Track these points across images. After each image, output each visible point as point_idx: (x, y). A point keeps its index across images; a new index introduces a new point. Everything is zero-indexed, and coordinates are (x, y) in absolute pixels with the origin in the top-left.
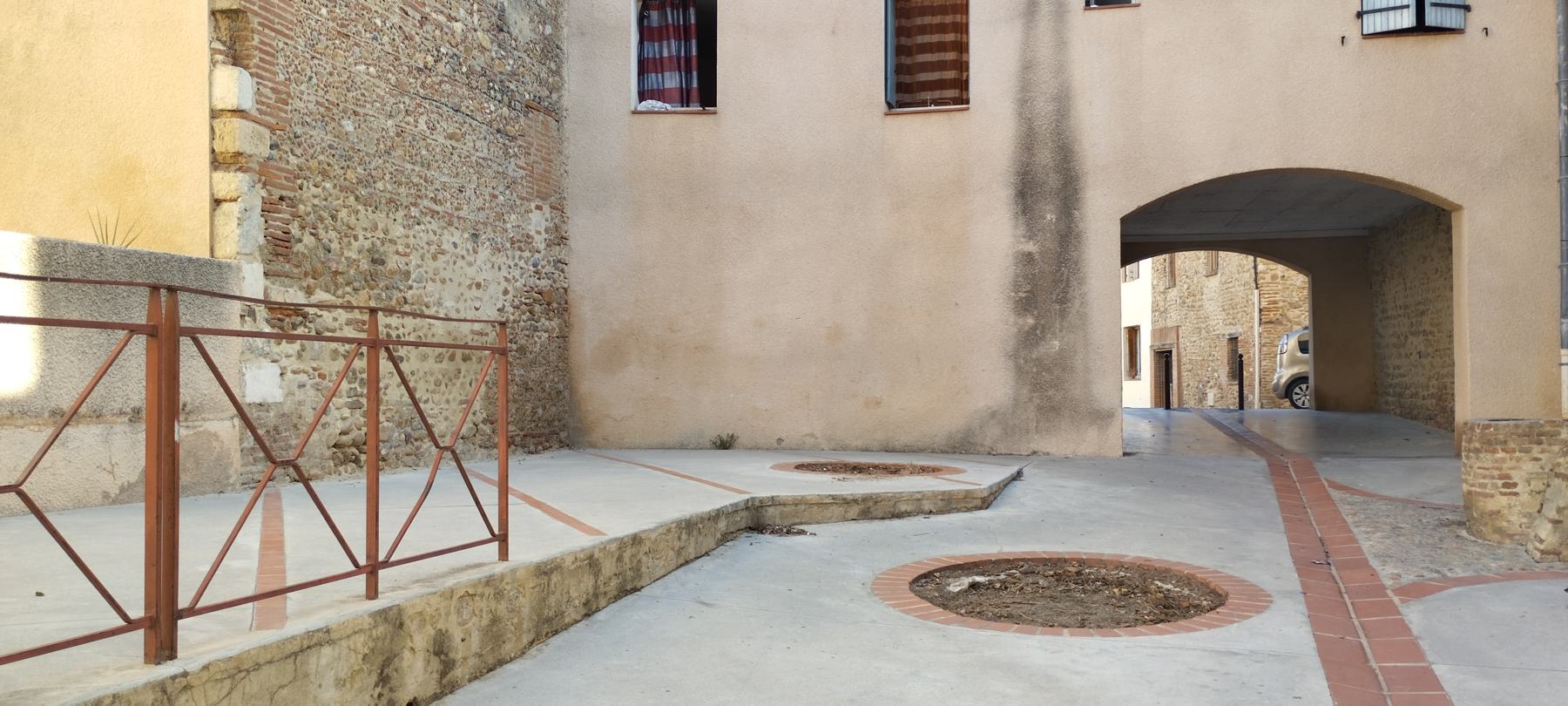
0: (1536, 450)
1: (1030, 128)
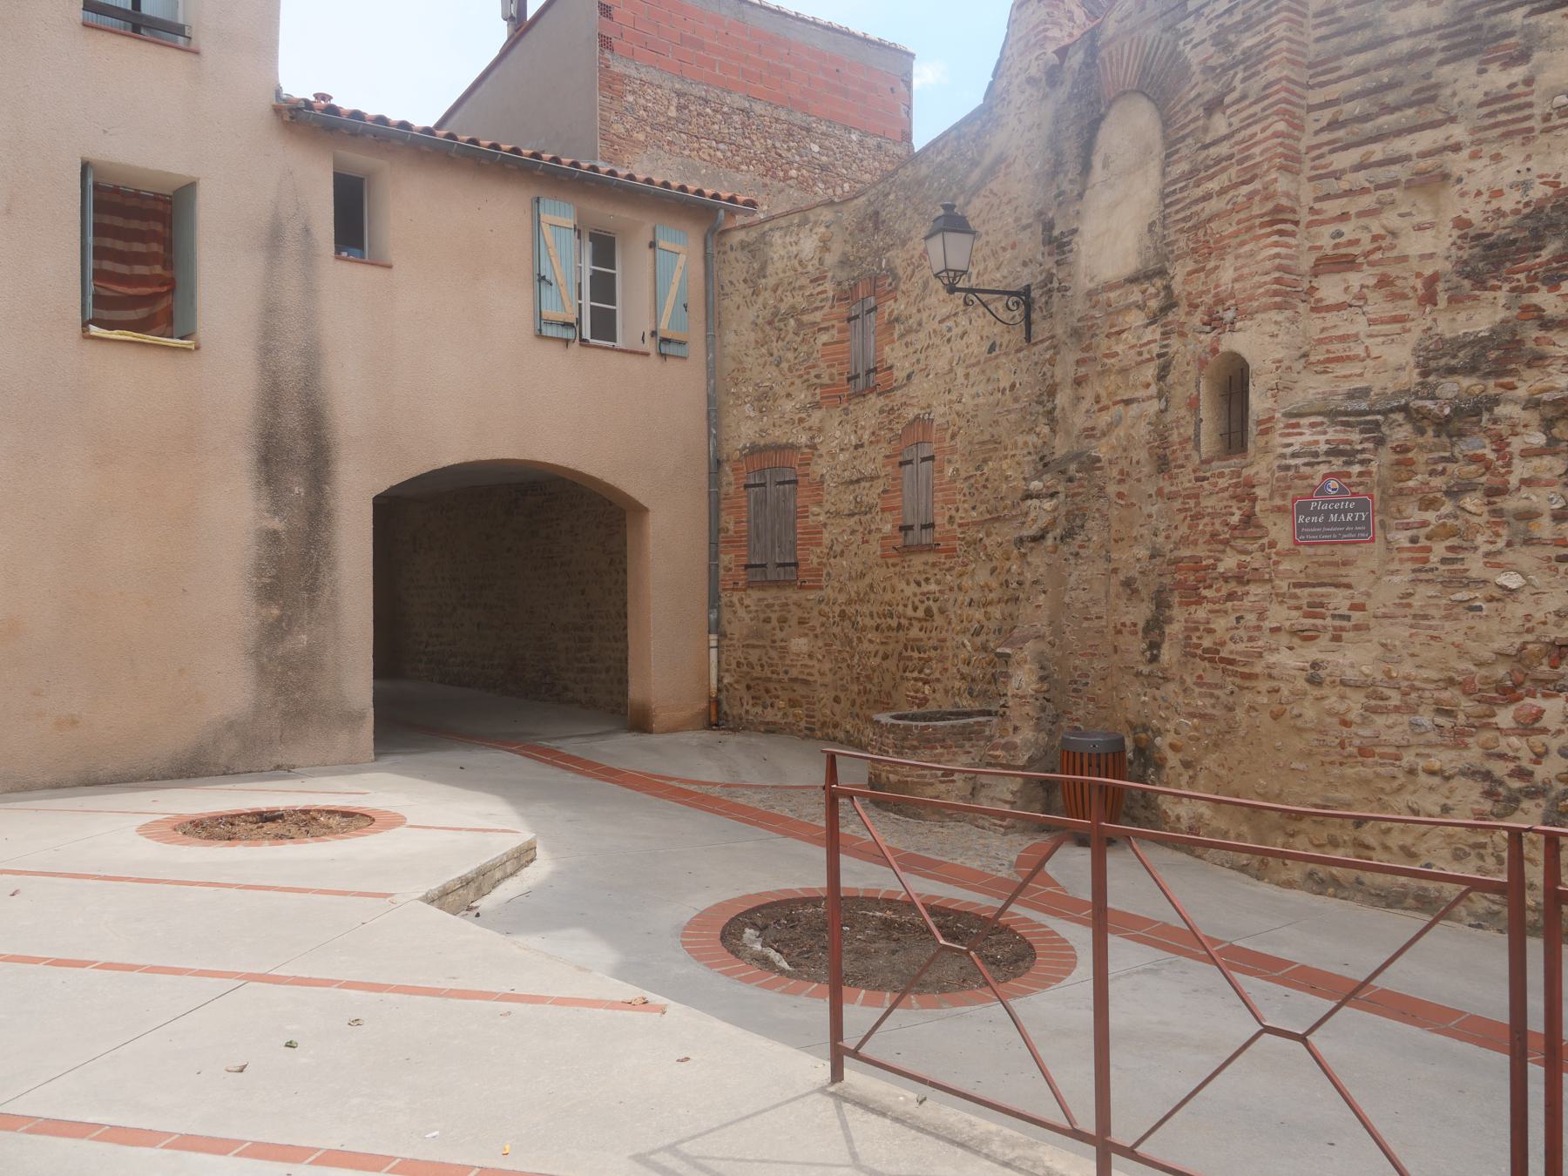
0: (967, 744)
1: (275, 384)
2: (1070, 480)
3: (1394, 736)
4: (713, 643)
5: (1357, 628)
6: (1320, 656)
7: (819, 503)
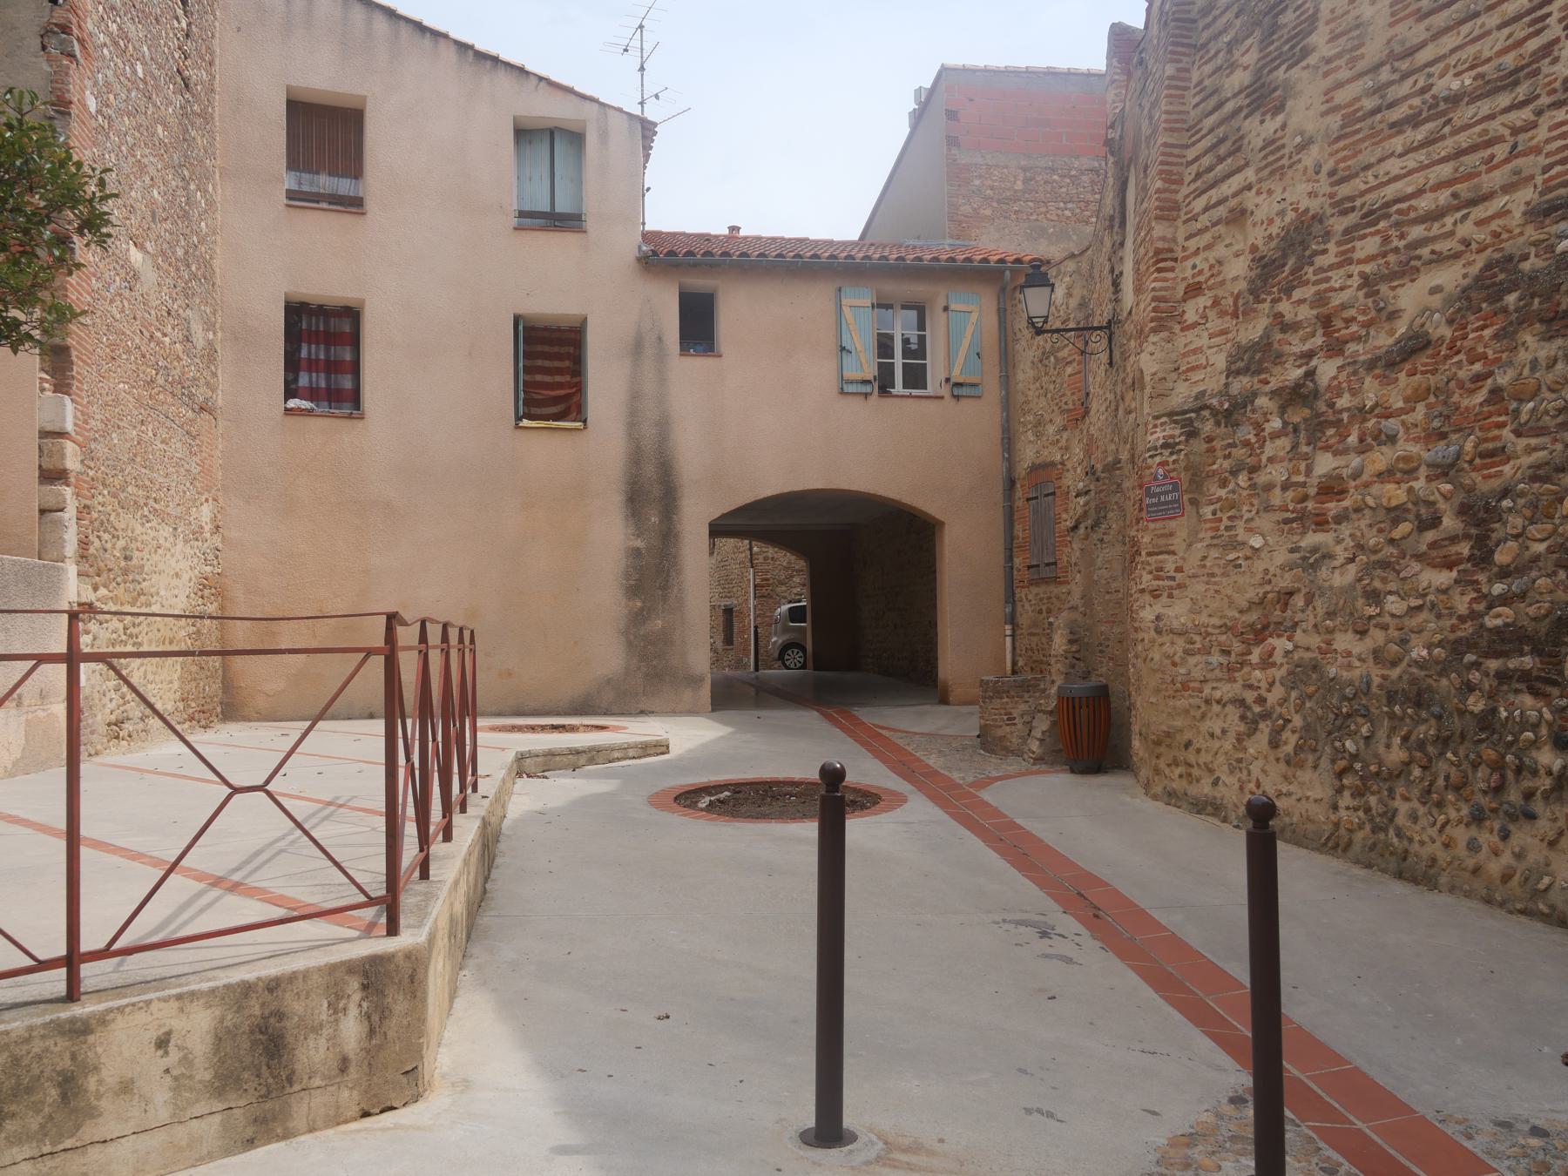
1: (638, 447)
2: (1098, 480)
3: (1197, 674)
4: (1008, 632)
5: (1179, 586)
6: (1162, 611)
7: (1066, 510)
